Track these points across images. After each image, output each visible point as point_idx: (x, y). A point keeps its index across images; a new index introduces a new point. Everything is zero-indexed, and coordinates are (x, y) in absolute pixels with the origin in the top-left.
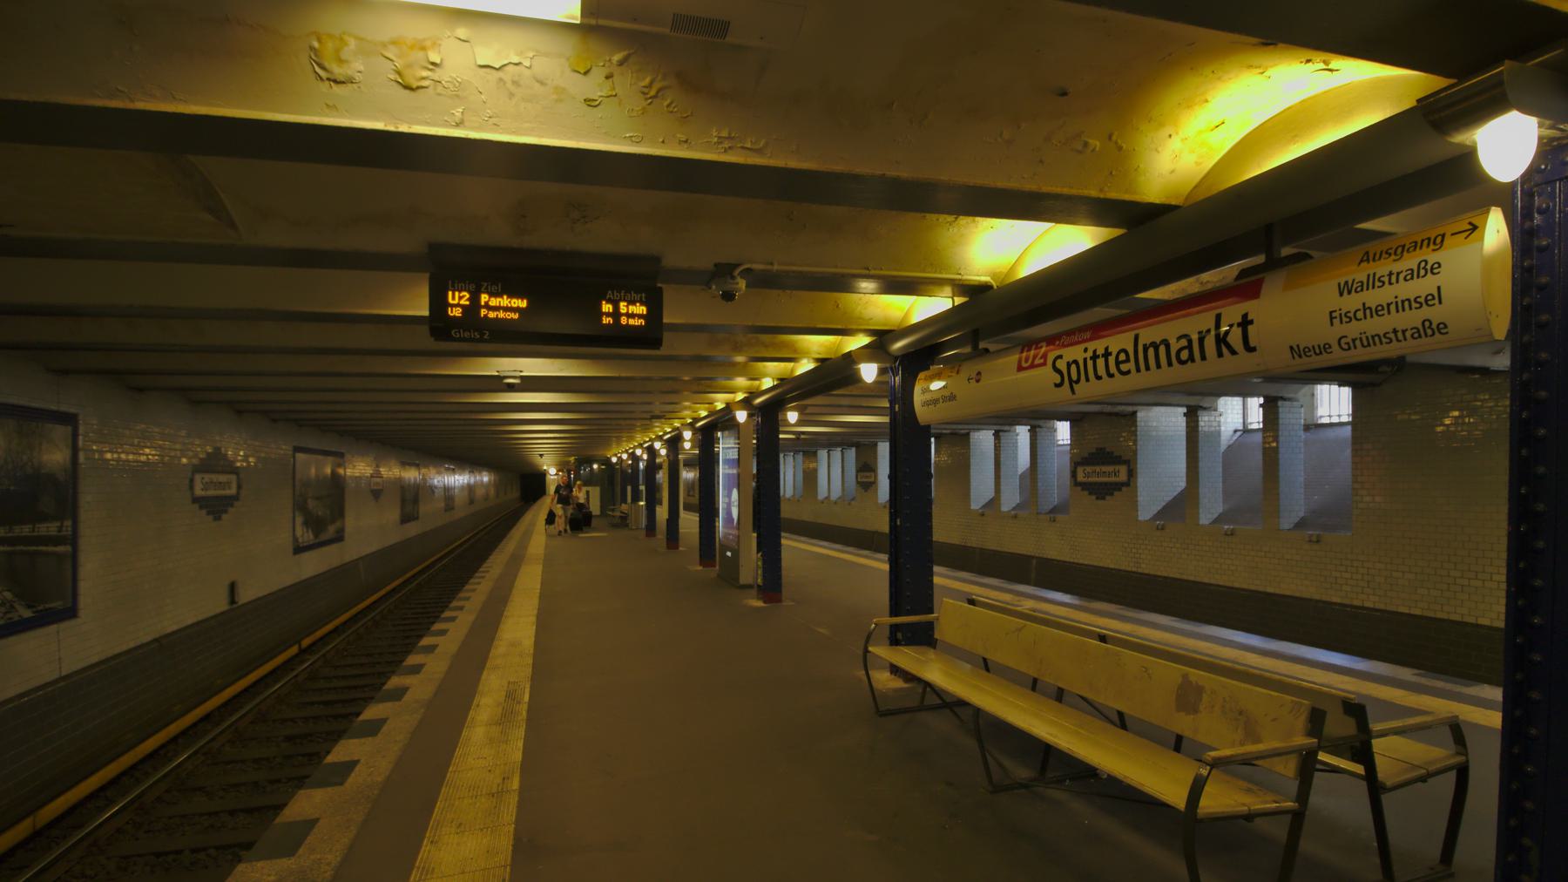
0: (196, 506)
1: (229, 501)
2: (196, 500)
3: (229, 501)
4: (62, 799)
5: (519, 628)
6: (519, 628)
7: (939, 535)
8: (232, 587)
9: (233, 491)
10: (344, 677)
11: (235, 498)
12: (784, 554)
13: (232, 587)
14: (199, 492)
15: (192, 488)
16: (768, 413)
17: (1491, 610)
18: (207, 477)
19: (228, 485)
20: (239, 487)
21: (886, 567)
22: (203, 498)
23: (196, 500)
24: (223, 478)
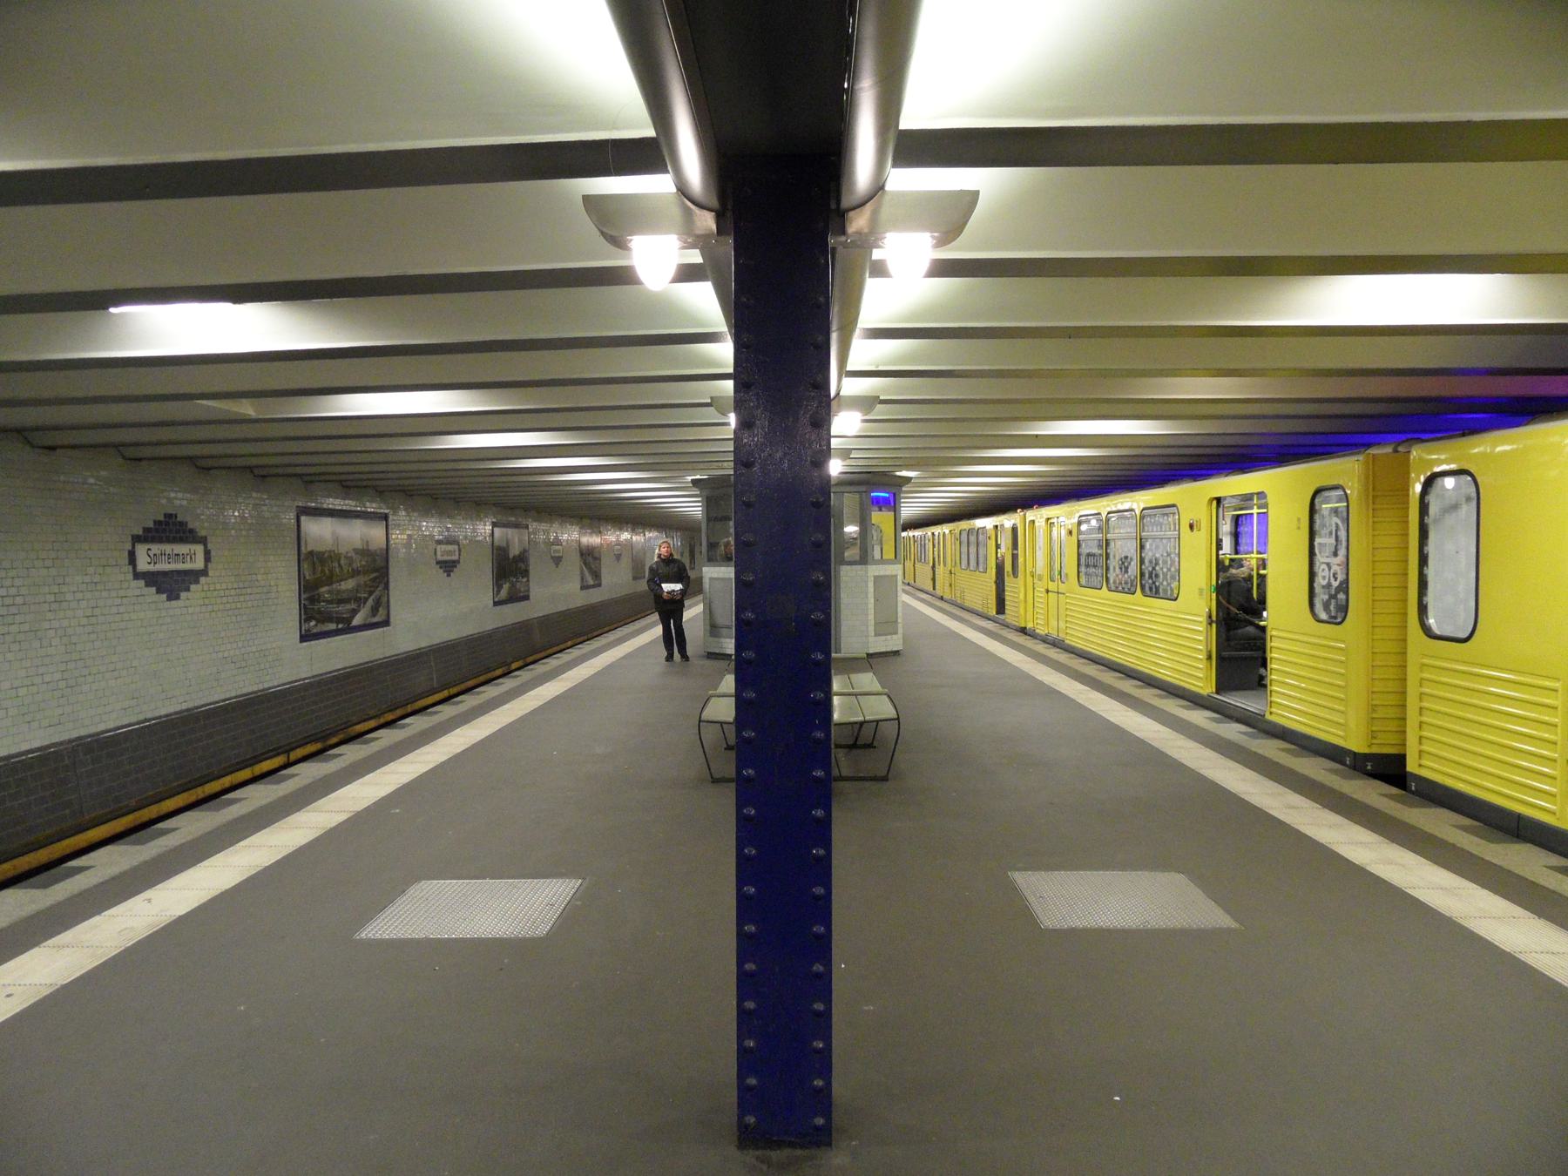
1: (194, 576)
3: (194, 576)
20: (207, 558)
24: (182, 549)
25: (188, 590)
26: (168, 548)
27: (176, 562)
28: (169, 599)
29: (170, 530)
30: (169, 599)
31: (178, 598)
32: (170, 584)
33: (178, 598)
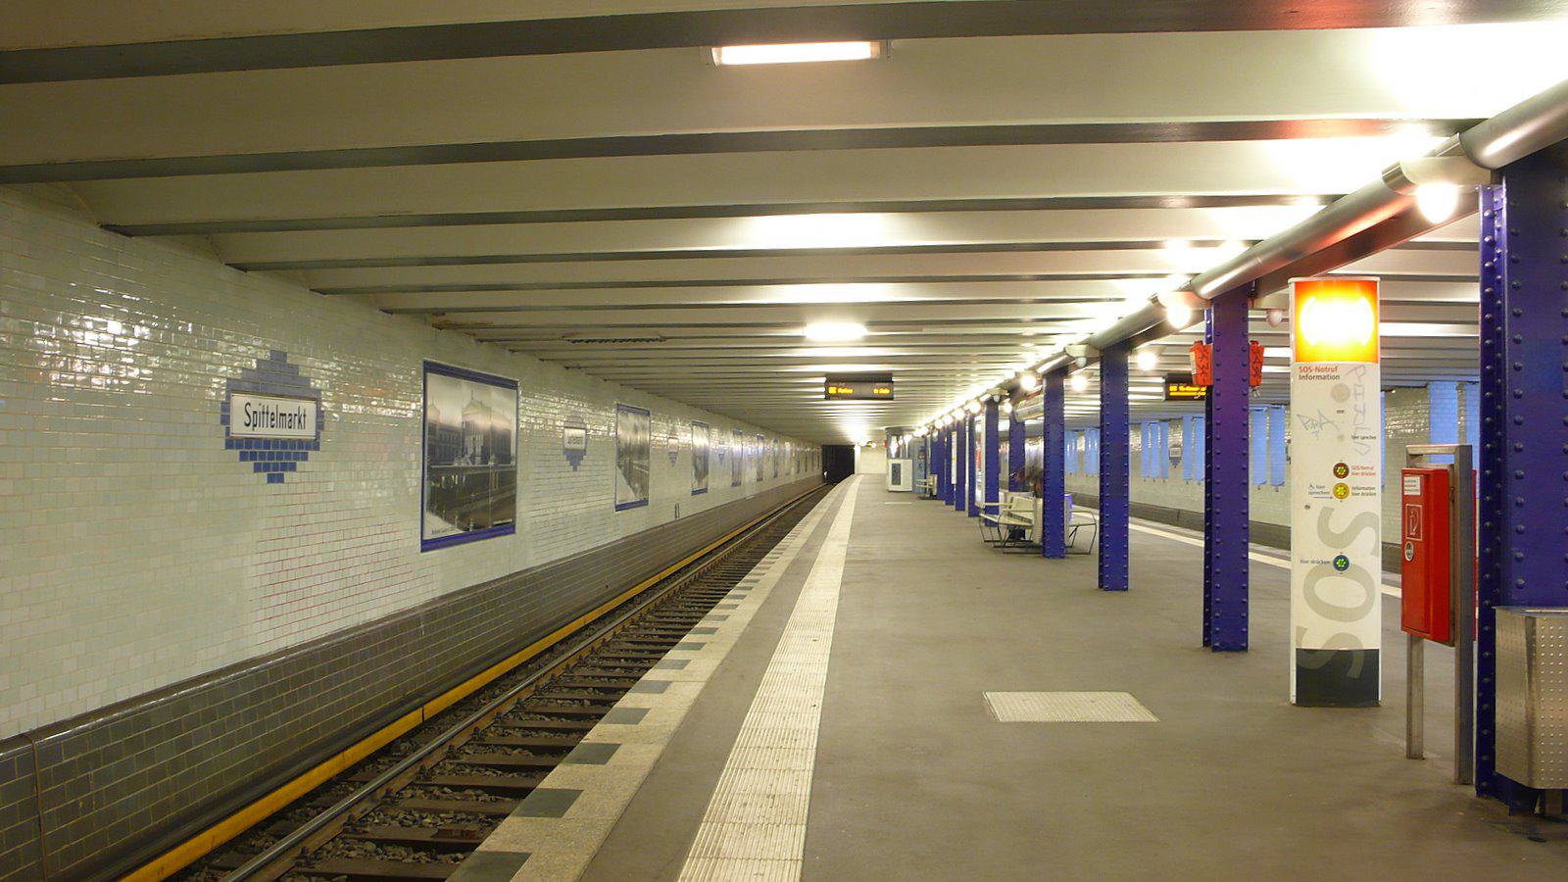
0: (236, 453)
1: (302, 449)
2: (230, 443)
3: (302, 449)
4: (206, 835)
5: (822, 593)
6: (822, 593)
7: (1253, 516)
8: (677, 507)
9: (308, 432)
10: (665, 629)
11: (315, 445)
12: (1131, 540)
13: (677, 507)
14: (238, 429)
15: (225, 420)
16: (1233, 305)
17: (1200, 508)
18: (257, 403)
19: (300, 419)
21: (1202, 544)
22: (249, 442)
23: (1170, 458)
25: (293, 468)
26: (271, 404)
27: (281, 426)
28: (271, 479)
29: (276, 378)
30: (271, 479)
31: (281, 479)
32: (273, 458)
33: (281, 479)
